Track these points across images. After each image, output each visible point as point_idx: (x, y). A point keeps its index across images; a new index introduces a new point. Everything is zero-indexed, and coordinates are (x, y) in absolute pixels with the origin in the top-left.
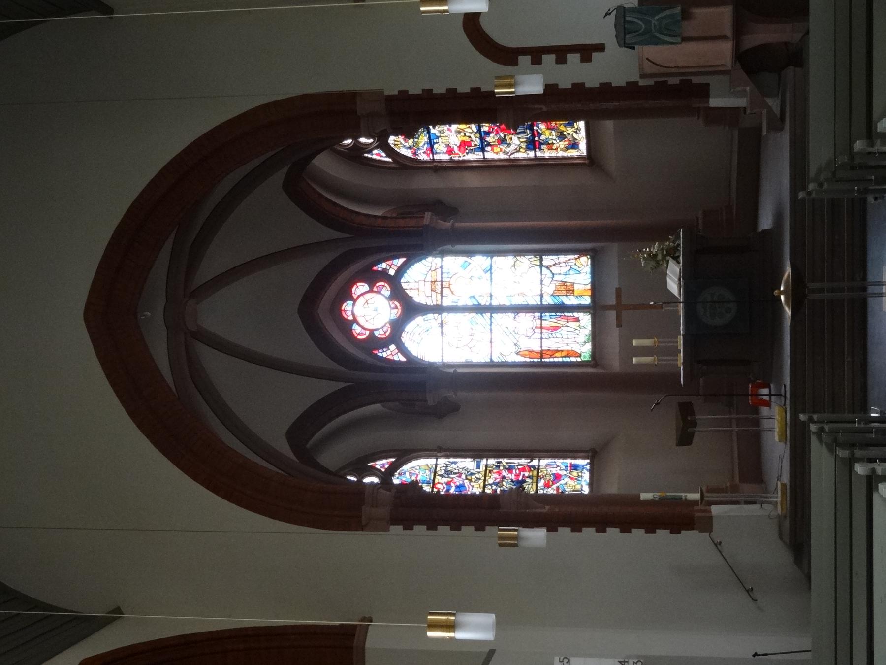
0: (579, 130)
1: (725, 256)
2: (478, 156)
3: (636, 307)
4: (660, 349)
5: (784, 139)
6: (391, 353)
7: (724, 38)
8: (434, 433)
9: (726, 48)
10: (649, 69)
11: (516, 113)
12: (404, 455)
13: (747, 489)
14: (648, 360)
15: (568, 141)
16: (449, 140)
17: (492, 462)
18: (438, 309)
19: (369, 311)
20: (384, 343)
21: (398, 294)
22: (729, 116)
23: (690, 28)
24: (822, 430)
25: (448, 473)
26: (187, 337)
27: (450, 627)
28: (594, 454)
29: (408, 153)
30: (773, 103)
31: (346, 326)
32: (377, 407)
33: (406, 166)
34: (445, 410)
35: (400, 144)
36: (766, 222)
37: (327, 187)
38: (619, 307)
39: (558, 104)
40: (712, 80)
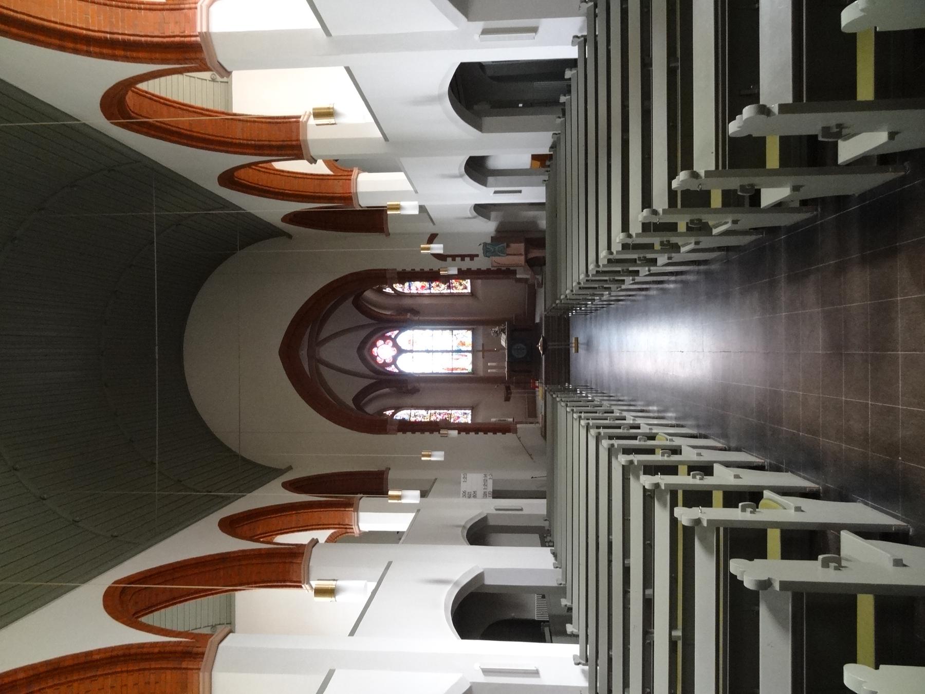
0: (468, 283)
1: (521, 330)
2: (428, 291)
3: (490, 351)
4: (498, 367)
5: (542, 290)
6: (392, 369)
7: (521, 254)
8: (409, 400)
9: (522, 258)
10: (495, 264)
11: (446, 279)
12: (398, 409)
13: (531, 420)
14: (494, 371)
15: (464, 287)
16: (417, 287)
17: (433, 411)
18: (411, 351)
19: (383, 352)
20: (389, 365)
21: (395, 345)
22: (525, 281)
23: (509, 251)
24: (580, 417)
25: (415, 416)
26: (316, 360)
27: (430, 456)
28: (473, 408)
29: (401, 290)
30: (539, 277)
31: (374, 358)
32: (387, 390)
33: (399, 295)
34: (414, 391)
35: (398, 287)
36: (537, 320)
37: (375, 306)
38: (483, 351)
39: (462, 275)
40: (517, 269)
